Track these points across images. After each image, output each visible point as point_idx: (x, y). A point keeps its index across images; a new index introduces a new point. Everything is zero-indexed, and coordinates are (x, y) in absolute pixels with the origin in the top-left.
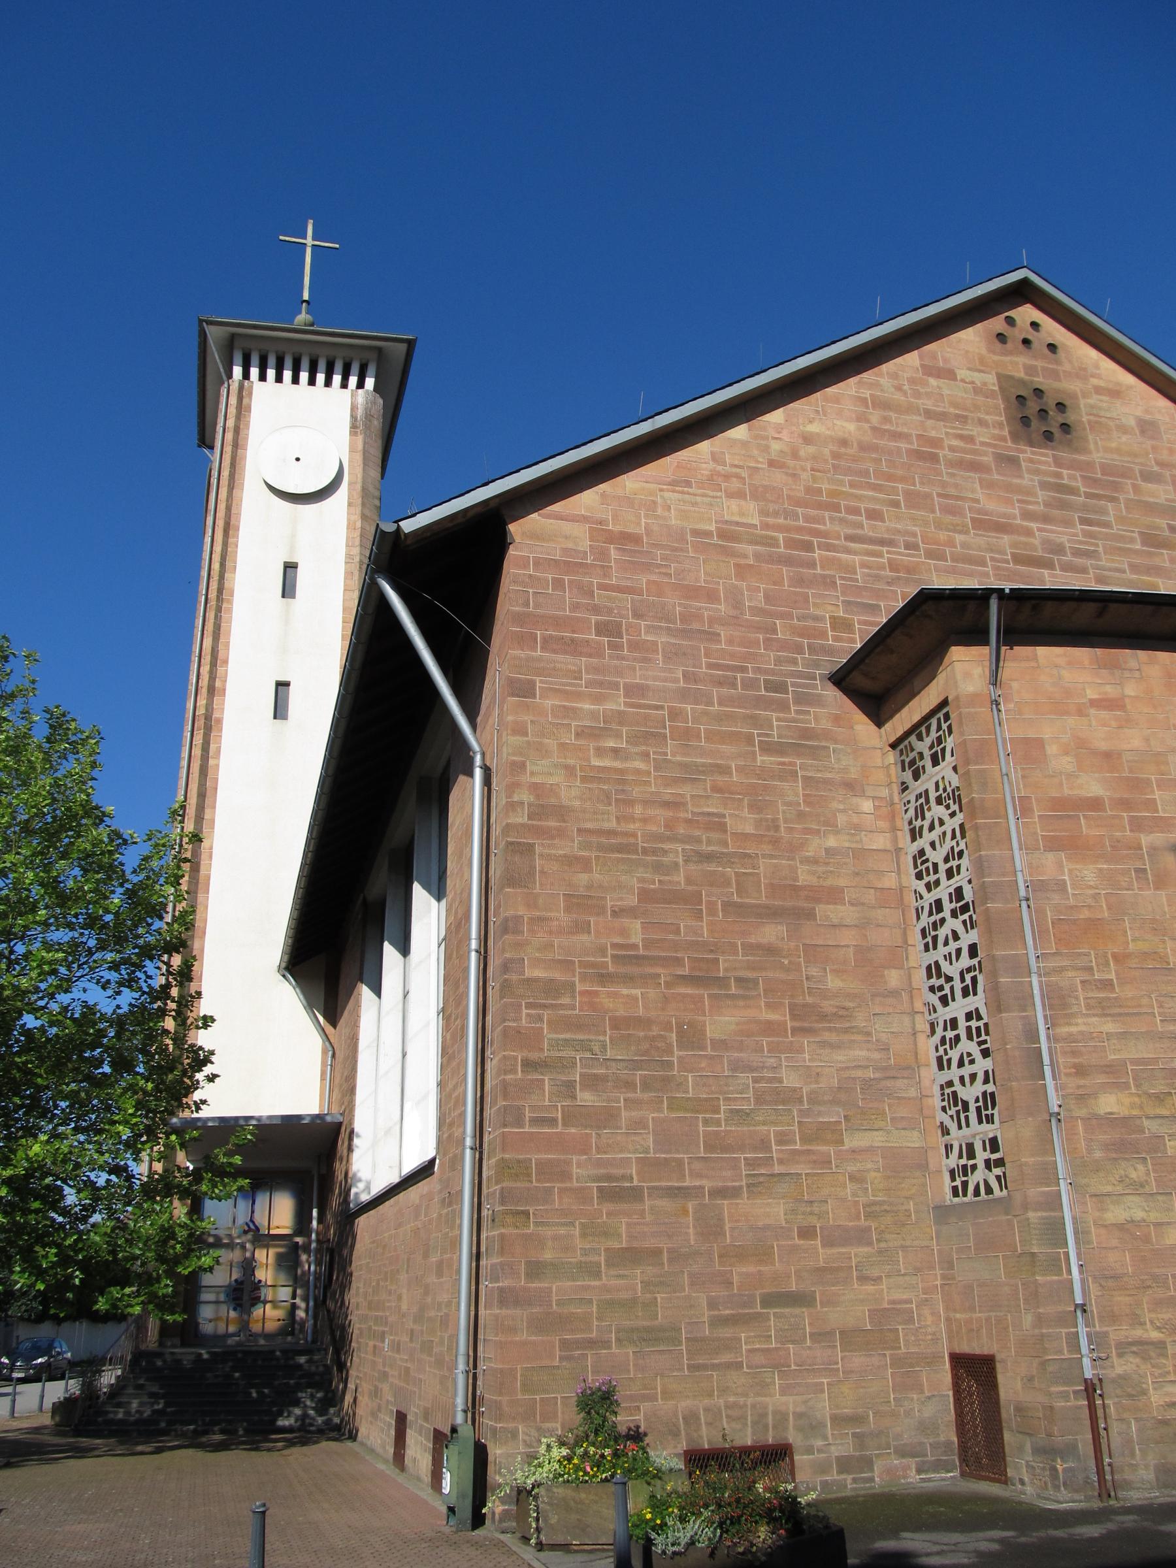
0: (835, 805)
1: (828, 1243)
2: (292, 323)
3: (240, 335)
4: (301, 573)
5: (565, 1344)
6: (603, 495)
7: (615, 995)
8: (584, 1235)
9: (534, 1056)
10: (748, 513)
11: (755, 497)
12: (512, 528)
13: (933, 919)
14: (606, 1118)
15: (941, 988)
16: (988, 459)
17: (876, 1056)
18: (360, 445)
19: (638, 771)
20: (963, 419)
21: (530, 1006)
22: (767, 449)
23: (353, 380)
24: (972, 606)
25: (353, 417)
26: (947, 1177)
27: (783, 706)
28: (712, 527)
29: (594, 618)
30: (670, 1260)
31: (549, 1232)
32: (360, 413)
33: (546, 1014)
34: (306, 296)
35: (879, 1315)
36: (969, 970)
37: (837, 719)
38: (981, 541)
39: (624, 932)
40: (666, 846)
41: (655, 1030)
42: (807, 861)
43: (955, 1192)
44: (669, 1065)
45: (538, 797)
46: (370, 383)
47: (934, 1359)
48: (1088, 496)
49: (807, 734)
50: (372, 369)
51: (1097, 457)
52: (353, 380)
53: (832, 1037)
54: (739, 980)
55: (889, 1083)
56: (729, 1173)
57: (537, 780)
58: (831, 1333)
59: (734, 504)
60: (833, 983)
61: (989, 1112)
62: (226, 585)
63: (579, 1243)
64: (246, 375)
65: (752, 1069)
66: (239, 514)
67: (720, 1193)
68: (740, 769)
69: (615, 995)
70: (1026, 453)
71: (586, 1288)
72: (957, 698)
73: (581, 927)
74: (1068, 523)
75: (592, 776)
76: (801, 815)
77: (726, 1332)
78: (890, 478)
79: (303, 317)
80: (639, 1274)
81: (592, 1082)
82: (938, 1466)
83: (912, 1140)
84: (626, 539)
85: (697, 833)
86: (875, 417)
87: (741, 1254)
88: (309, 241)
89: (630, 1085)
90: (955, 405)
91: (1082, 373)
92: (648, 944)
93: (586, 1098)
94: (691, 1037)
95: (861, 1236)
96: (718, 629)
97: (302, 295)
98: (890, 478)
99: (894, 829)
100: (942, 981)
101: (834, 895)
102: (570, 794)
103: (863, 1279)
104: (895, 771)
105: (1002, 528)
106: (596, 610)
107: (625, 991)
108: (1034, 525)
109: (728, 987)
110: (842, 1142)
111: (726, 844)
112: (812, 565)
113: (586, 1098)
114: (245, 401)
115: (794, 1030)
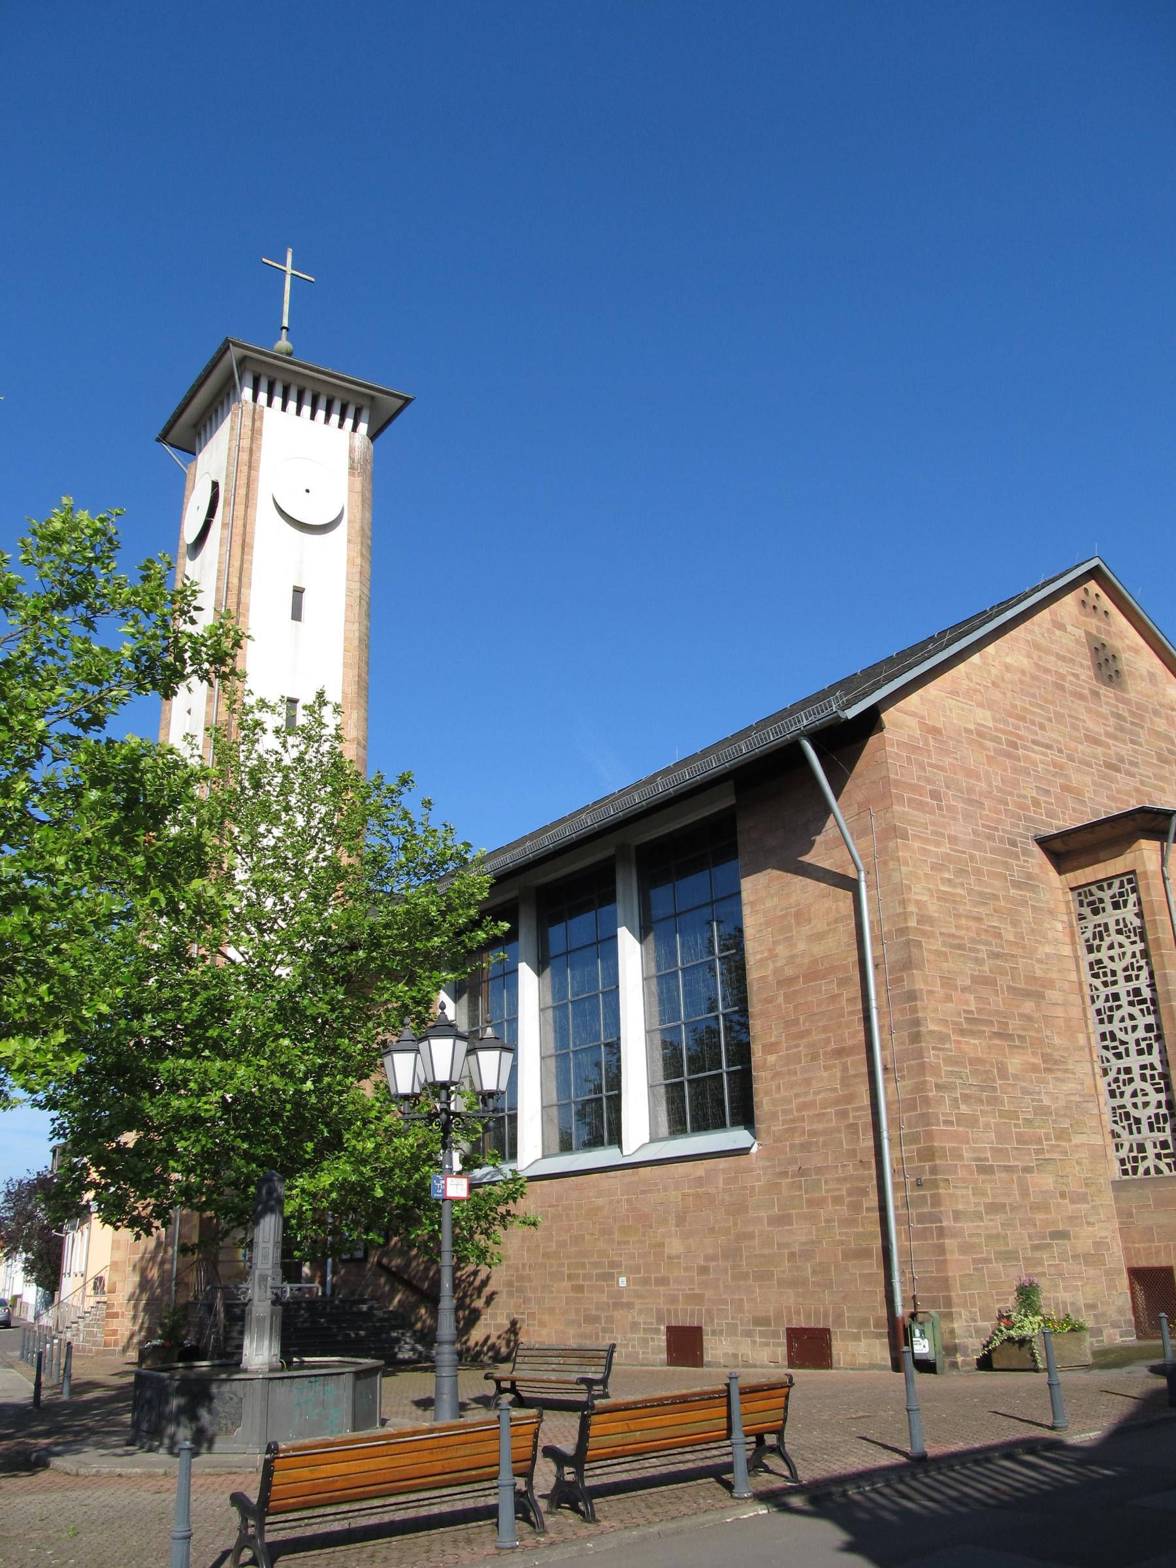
0: (1047, 926)
1: (1072, 1202)
2: (272, 348)
3: (251, 358)
4: (306, 597)
5: (974, 1260)
6: (921, 697)
7: (968, 1043)
8: (974, 1194)
9: (939, 1081)
10: (984, 717)
11: (990, 708)
12: (883, 716)
13: (1109, 1004)
14: (972, 1121)
15: (1115, 1048)
16: (1086, 692)
17: (1079, 1087)
18: (358, 487)
19: (960, 895)
20: (1072, 661)
21: (934, 1048)
22: (989, 672)
23: (349, 422)
24: (1161, 818)
25: (352, 459)
26: (1117, 1164)
27: (1017, 858)
28: (972, 727)
29: (929, 787)
30: (1011, 1210)
31: (959, 1192)
32: (357, 456)
33: (941, 1054)
34: (285, 323)
35: (1097, 1244)
36: (1144, 1039)
37: (1041, 866)
38: (1088, 750)
39: (967, 1003)
40: (978, 947)
41: (988, 1068)
42: (1040, 961)
43: (1125, 1172)
44: (994, 1089)
45: (919, 909)
46: (363, 427)
47: (1119, 1272)
48: (1133, 723)
49: (1030, 876)
50: (365, 414)
51: (1132, 696)
52: (349, 422)
53: (1059, 1075)
54: (1019, 1036)
55: (1085, 1105)
56: (1027, 1158)
57: (917, 897)
58: (1078, 1256)
59: (979, 711)
60: (1057, 1041)
61: (1161, 1125)
62: (243, 600)
63: (972, 1199)
64: (255, 398)
65: (1030, 1094)
66: (253, 533)
67: (1027, 1170)
68: (1005, 897)
69: (968, 1043)
70: (1103, 690)
71: (979, 1227)
72: (1145, 873)
73: (949, 998)
74: (1124, 742)
75: (943, 897)
76: (1033, 930)
77: (1037, 1254)
78: (1046, 701)
79: (283, 344)
80: (999, 1218)
81: (966, 1098)
82: (1128, 1333)
83: (1098, 1140)
84: (935, 731)
85: (990, 939)
86: (1035, 654)
87: (1036, 1208)
88: (288, 268)
89: (981, 1101)
90: (1068, 651)
91: (1121, 635)
92: (979, 1010)
93: (964, 1108)
94: (1003, 1073)
95: (1082, 1198)
96: (983, 800)
97: (282, 322)
98: (1046, 701)
99: (1073, 943)
100: (1117, 1043)
101: (1050, 984)
102: (933, 909)
103: (1088, 1223)
104: (1074, 906)
105: (1097, 742)
106: (928, 781)
107: (972, 1041)
108: (1111, 742)
109: (1013, 1040)
110: (1070, 1140)
111: (1002, 947)
112: (1018, 759)
113: (964, 1108)
114: (257, 424)
115: (1045, 1069)
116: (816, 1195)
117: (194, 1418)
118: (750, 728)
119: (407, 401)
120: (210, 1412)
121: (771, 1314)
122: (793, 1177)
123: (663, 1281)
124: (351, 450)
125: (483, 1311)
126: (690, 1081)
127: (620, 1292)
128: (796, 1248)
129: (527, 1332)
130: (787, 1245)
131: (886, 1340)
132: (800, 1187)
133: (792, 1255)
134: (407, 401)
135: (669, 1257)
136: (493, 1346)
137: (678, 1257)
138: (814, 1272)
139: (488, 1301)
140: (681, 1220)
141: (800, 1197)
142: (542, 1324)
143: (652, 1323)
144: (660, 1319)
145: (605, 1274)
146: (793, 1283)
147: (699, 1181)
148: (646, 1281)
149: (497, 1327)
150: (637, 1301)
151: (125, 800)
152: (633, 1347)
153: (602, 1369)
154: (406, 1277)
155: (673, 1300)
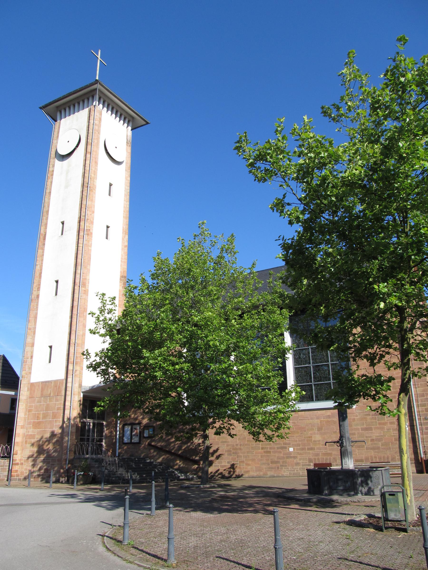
25: (127, 139)
116: (383, 421)
117: (367, 484)
118: (41, 278)
119: (147, 123)
120: (371, 481)
121: (364, 458)
122: (372, 416)
123: (312, 449)
124: (127, 136)
125: (215, 461)
126: (315, 385)
127: (290, 453)
128: (374, 438)
129: (240, 468)
130: (370, 437)
131: (414, 465)
132: (376, 419)
133: (372, 440)
134: (147, 123)
135: (315, 441)
136: (221, 473)
137: (320, 441)
138: (382, 445)
139: (218, 457)
140: (319, 429)
141: (376, 422)
142: (248, 465)
143: (306, 463)
144: (310, 461)
145: (282, 447)
146: (373, 449)
147: (329, 417)
148: (303, 449)
149: (222, 466)
150: (298, 456)
151: (417, 250)
152: (297, 471)
153: (400, 470)
154: (167, 449)
155: (318, 455)
